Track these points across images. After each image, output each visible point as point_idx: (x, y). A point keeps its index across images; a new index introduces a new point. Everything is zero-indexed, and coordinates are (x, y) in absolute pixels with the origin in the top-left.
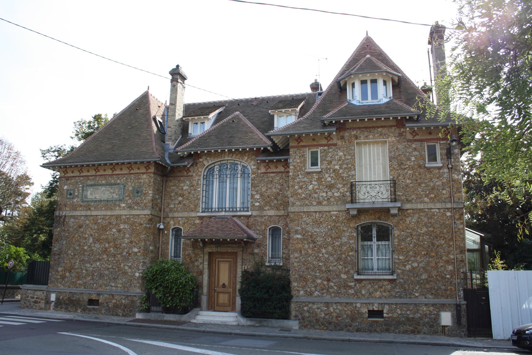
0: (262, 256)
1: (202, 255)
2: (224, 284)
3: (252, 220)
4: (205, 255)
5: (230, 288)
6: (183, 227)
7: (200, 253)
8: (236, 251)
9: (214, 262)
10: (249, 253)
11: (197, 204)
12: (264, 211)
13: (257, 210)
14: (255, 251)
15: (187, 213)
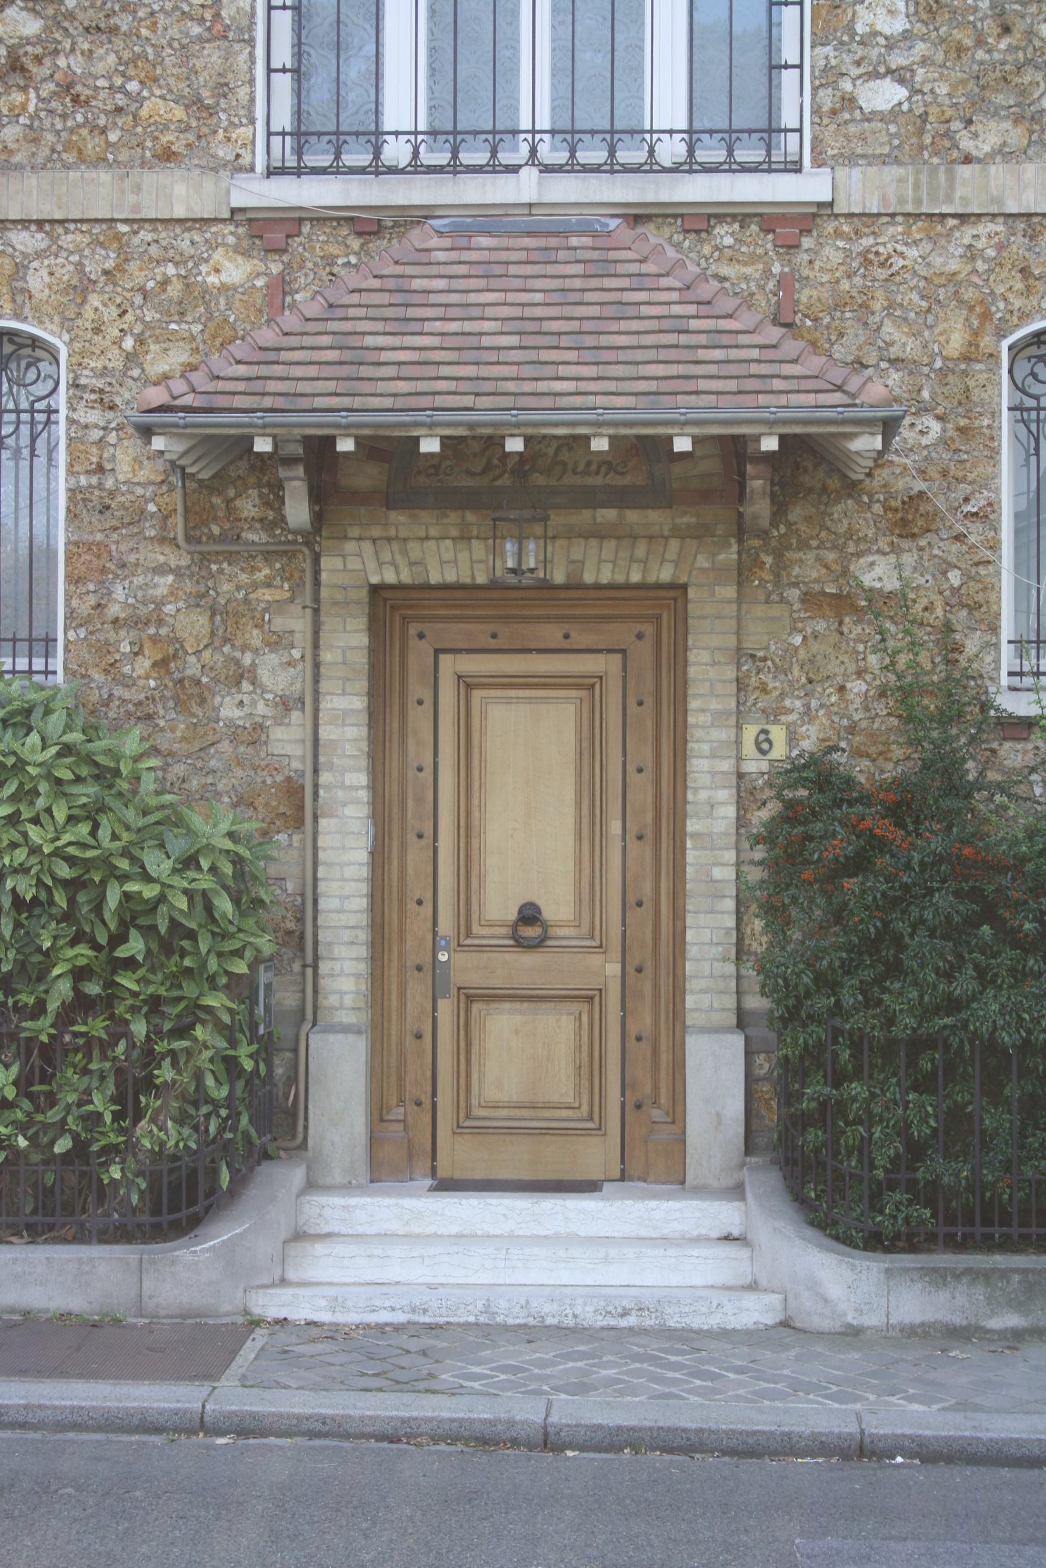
0: (948, 628)
1: (298, 623)
2: (529, 915)
3: (832, 254)
4: (329, 623)
5: (601, 947)
6: (67, 324)
7: (267, 595)
8: (666, 574)
9: (418, 690)
10: (812, 600)
11: (223, 89)
12: (965, 171)
13: (884, 160)
14: (868, 580)
15: (104, 176)
